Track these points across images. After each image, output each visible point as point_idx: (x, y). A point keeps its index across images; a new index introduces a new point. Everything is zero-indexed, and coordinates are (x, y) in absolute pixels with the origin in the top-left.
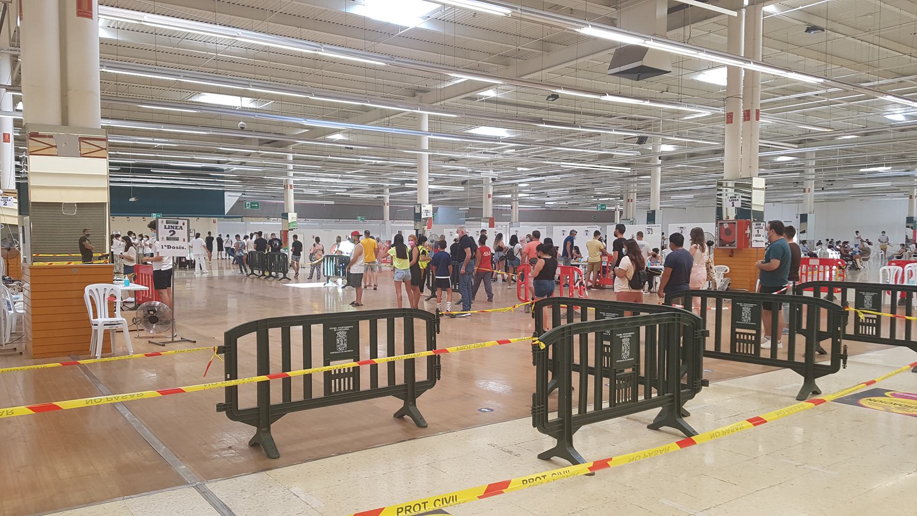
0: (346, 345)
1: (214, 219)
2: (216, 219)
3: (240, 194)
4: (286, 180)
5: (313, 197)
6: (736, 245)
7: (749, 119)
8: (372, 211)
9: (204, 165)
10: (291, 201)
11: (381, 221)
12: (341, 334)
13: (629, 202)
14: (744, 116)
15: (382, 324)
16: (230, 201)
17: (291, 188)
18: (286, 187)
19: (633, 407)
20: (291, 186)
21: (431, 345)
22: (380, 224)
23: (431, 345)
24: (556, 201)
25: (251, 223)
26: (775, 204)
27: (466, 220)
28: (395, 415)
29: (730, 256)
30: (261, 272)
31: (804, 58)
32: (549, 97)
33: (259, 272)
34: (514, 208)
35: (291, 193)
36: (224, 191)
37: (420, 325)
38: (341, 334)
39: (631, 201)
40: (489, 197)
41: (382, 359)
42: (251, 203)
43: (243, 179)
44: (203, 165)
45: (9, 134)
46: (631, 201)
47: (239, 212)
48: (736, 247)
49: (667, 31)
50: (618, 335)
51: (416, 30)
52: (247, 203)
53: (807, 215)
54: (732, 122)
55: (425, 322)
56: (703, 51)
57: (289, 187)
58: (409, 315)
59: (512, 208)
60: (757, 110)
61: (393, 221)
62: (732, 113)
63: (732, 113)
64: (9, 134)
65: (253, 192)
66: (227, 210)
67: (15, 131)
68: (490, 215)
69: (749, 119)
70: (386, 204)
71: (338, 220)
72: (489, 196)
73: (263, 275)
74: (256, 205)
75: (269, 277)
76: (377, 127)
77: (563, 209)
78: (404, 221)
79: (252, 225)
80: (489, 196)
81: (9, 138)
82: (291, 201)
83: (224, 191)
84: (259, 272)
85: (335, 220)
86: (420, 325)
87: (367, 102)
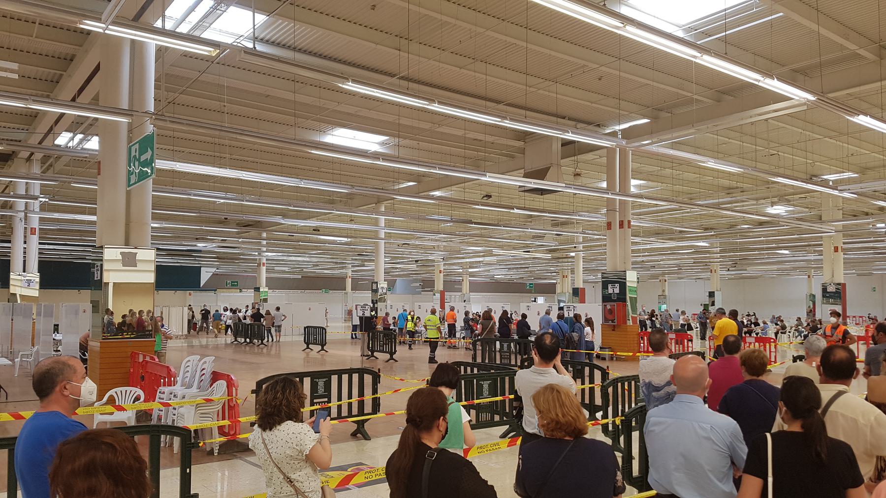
0: (323, 390)
1: (190, 291)
2: (192, 292)
3: (214, 270)
4: (260, 259)
5: (284, 272)
6: (616, 322)
7: (623, 228)
8: (334, 284)
9: (189, 248)
10: (264, 275)
11: (344, 291)
12: (321, 383)
13: (564, 277)
14: (620, 225)
15: (345, 377)
16: (205, 275)
17: (264, 266)
18: (259, 265)
19: (491, 424)
20: (264, 264)
21: (375, 391)
22: (342, 294)
23: (375, 391)
24: (503, 275)
25: (222, 294)
26: (697, 280)
27: (422, 291)
28: (351, 435)
29: (613, 330)
30: (260, 341)
31: (682, 172)
32: (484, 197)
33: (258, 342)
34: (465, 281)
35: (264, 269)
36: (201, 267)
37: (368, 379)
38: (321, 383)
39: (566, 277)
40: (440, 273)
41: (345, 401)
42: (232, 282)
43: (220, 257)
44: (189, 248)
45: (35, 228)
46: (566, 277)
47: (215, 284)
48: (616, 324)
49: (562, 159)
50: (480, 382)
51: (375, 152)
52: (228, 282)
53: (714, 292)
54: (611, 229)
55: (371, 376)
56: (571, 188)
57: (262, 264)
58: (361, 372)
59: (463, 281)
60: (628, 221)
61: (354, 291)
62: (611, 222)
63: (611, 222)
64: (35, 228)
65: (225, 269)
66: (201, 286)
67: (41, 224)
68: (441, 288)
69: (623, 228)
70: (348, 277)
71: (303, 291)
72: (440, 272)
73: (245, 341)
74: (236, 284)
75: (250, 343)
76: (341, 224)
77: (511, 282)
78: (364, 292)
79: (223, 296)
80: (440, 272)
81: (35, 231)
82: (264, 275)
83: (201, 267)
84: (258, 342)
85: (301, 291)
86: (368, 379)
87: (334, 210)
